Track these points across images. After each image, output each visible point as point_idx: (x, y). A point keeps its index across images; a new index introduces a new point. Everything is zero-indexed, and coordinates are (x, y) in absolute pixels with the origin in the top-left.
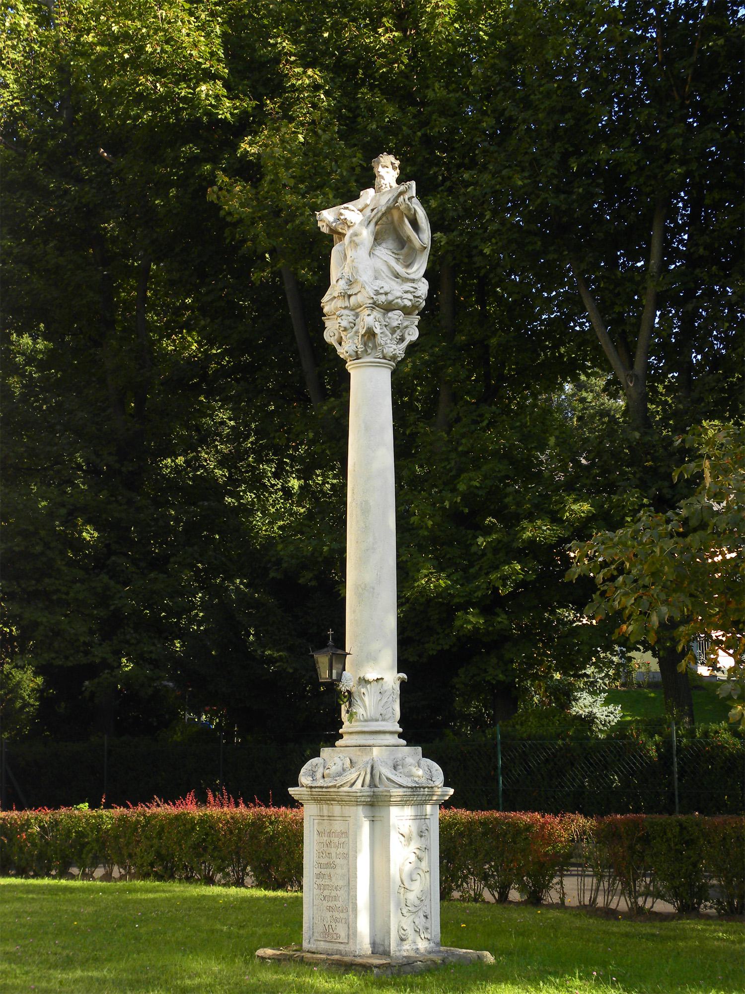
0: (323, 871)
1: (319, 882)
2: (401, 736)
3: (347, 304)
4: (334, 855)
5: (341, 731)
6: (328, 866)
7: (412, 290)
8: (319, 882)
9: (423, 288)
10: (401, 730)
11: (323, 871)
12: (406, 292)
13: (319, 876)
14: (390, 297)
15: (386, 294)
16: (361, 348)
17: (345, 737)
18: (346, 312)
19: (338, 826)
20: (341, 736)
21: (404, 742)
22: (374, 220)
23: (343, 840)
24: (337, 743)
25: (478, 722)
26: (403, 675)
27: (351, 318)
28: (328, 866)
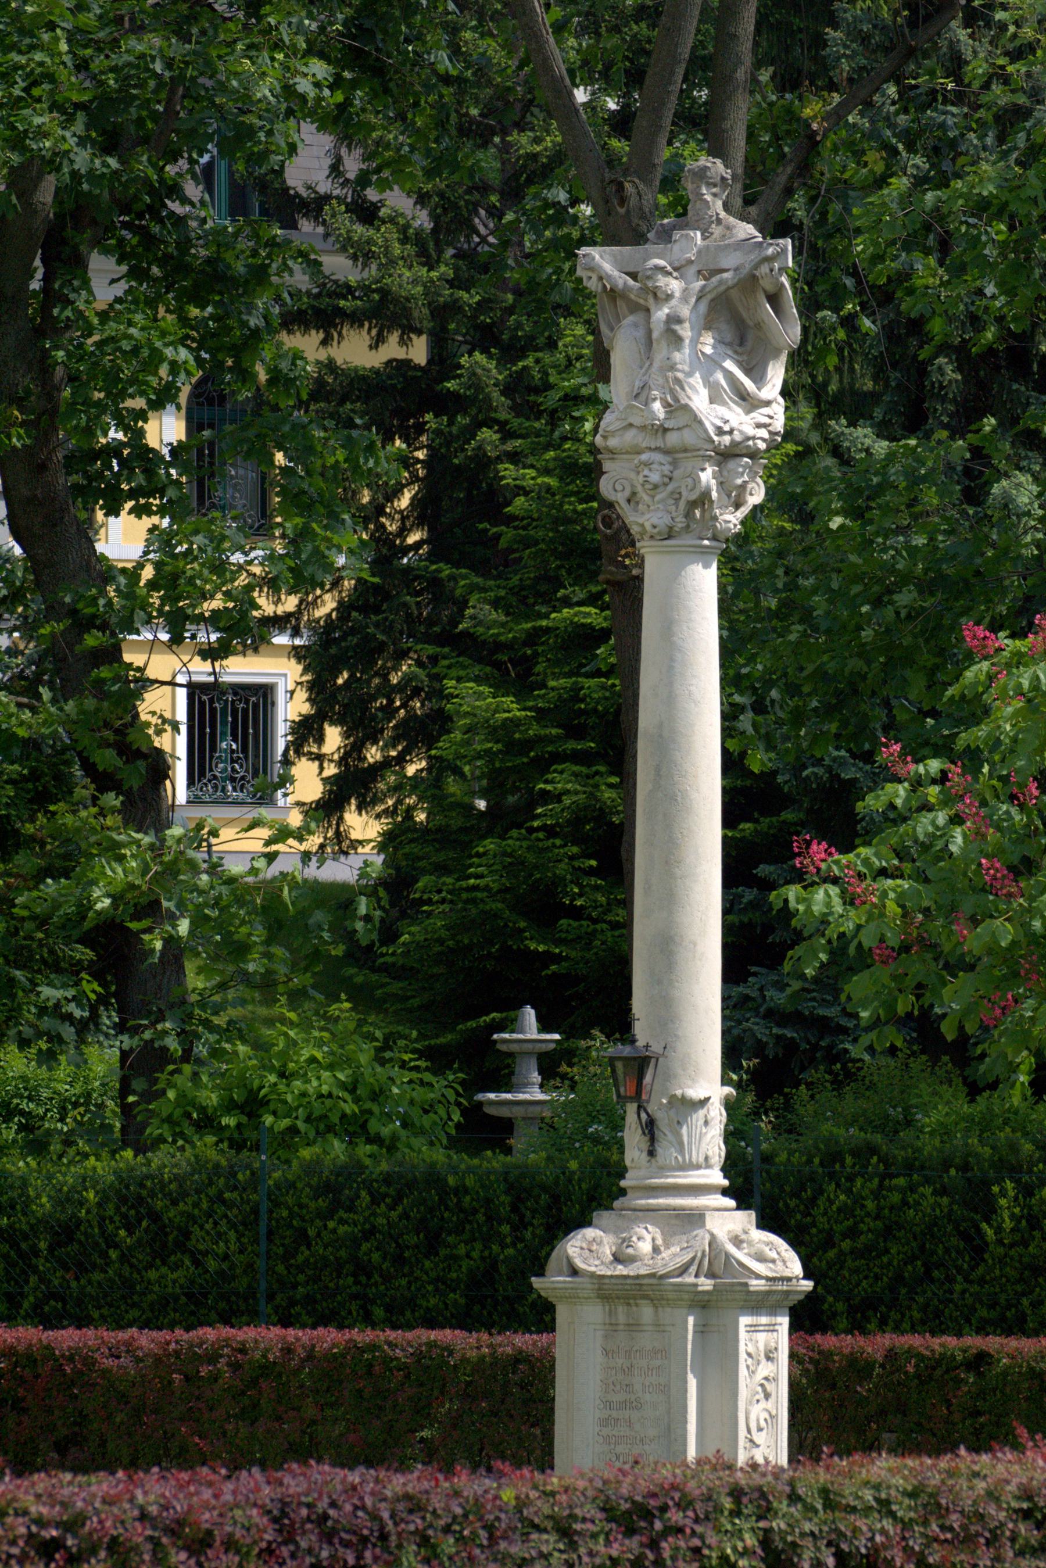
0: (614, 1414)
1: (606, 1431)
2: (725, 1192)
3: (659, 443)
4: (638, 1387)
5: (623, 1183)
6: (623, 1405)
7: (767, 420)
8: (606, 1431)
9: (777, 415)
10: (726, 1183)
11: (614, 1414)
12: (759, 426)
13: (604, 1422)
14: (737, 437)
15: (731, 432)
16: (680, 522)
17: (630, 1194)
18: (658, 457)
19: (646, 1340)
20: (623, 1192)
21: (732, 1203)
22: (710, 297)
23: (658, 1363)
24: (616, 1204)
25: (88, 1212)
26: (728, 1090)
27: (667, 469)
28: (623, 1405)
